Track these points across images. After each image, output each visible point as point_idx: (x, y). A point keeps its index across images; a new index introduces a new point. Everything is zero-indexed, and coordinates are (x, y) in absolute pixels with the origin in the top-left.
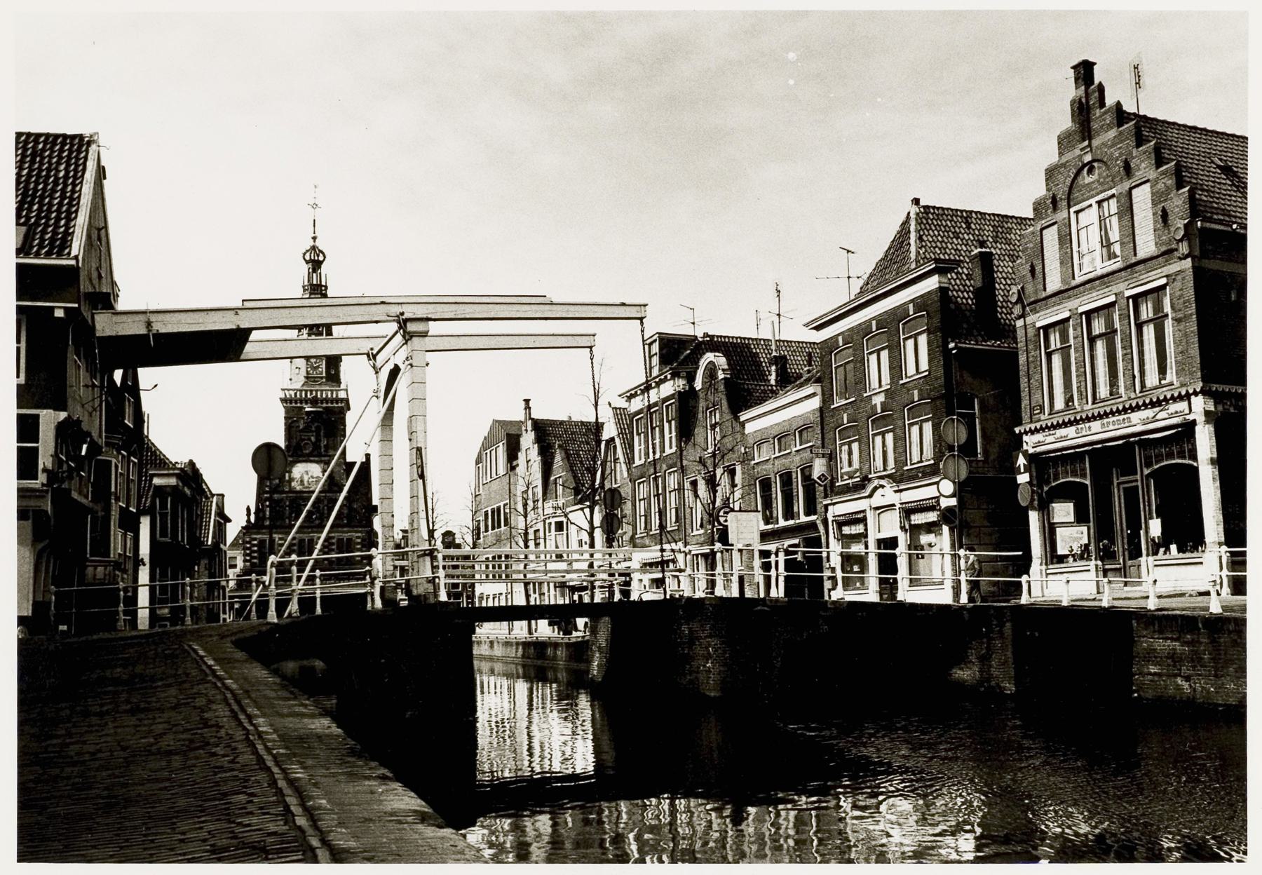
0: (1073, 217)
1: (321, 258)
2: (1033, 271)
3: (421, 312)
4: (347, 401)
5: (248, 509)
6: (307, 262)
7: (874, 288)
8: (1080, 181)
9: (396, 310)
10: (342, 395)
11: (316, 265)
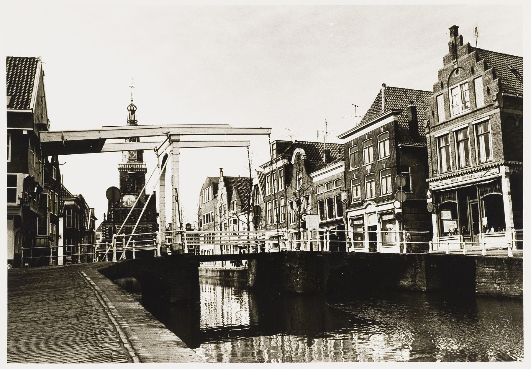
0: (450, 91)
1: (135, 109)
2: (433, 114)
3: (176, 131)
4: (146, 169)
5: (105, 215)
6: (129, 111)
7: (367, 121)
8: (453, 76)
9: (166, 131)
10: (144, 166)
11: (133, 112)
